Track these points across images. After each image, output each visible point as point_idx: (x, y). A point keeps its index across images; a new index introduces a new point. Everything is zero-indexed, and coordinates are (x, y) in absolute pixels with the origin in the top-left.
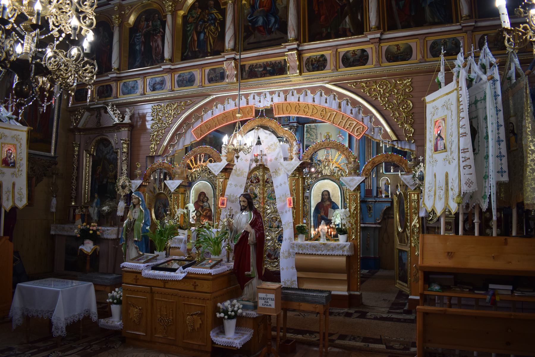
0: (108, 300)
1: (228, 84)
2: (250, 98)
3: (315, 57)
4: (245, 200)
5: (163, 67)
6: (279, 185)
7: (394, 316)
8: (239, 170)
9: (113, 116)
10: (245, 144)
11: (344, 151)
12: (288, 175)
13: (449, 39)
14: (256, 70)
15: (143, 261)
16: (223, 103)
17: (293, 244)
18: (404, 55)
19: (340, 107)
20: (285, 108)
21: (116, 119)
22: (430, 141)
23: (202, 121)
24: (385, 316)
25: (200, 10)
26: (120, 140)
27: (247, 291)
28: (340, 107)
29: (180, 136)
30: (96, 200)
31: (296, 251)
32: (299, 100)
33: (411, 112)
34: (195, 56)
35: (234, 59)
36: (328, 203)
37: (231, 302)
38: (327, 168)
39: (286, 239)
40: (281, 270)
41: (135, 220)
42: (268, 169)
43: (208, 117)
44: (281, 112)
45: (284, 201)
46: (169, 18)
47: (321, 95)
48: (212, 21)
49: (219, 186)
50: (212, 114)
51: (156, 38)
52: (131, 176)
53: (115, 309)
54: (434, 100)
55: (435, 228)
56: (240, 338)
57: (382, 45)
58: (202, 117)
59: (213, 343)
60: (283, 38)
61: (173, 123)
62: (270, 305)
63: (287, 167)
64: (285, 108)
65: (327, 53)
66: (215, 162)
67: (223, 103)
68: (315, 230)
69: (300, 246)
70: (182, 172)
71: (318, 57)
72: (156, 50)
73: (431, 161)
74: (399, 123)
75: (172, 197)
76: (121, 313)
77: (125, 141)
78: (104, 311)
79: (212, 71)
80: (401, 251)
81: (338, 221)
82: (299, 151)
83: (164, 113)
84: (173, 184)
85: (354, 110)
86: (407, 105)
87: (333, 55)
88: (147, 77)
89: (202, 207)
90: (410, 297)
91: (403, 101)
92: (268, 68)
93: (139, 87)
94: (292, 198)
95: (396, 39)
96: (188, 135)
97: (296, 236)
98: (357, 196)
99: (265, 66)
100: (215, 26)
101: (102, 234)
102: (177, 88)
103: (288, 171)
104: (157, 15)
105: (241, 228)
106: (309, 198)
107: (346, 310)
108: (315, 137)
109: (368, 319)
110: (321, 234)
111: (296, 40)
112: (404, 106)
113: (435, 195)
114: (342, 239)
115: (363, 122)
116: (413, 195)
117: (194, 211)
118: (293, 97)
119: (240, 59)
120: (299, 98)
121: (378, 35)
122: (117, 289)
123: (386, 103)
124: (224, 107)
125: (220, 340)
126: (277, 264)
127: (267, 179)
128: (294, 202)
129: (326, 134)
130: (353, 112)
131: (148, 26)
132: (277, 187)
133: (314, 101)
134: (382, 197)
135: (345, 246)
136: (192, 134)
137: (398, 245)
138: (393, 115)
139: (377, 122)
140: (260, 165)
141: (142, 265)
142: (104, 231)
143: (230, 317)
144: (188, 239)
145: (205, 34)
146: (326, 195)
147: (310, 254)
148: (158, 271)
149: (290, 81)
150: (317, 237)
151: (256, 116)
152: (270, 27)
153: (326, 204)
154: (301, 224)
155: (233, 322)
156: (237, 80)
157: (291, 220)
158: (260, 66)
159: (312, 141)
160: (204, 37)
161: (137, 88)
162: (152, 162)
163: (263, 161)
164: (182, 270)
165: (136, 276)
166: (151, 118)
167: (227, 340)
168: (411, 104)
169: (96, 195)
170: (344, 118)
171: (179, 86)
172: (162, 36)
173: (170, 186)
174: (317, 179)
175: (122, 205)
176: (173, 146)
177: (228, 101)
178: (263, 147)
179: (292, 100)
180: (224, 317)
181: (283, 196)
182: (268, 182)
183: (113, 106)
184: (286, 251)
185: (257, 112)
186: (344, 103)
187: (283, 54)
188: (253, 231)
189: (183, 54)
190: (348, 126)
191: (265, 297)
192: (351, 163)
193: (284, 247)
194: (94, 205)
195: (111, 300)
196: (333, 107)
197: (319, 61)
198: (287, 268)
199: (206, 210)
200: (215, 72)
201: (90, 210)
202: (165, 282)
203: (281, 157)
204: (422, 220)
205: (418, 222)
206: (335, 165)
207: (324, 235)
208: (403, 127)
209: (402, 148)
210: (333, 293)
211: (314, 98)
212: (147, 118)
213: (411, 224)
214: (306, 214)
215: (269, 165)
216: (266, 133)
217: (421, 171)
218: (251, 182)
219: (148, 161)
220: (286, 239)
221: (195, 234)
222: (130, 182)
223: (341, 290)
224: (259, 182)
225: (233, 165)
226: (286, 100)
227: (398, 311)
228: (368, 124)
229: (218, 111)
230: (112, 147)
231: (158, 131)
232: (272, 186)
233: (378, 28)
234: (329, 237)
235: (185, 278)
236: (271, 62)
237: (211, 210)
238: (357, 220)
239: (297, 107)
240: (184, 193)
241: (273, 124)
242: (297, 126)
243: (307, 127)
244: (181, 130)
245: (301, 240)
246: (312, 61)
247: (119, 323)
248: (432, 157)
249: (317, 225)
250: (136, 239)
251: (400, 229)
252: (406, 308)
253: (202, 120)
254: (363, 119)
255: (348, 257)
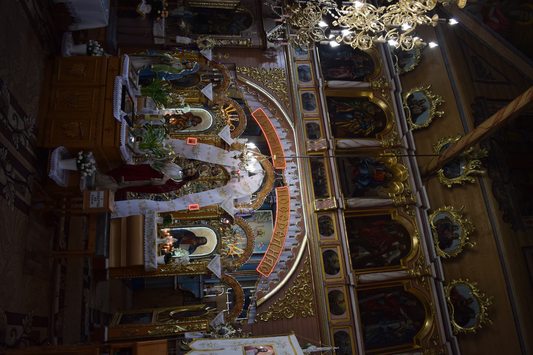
0: (91, 41)
1: (306, 143)
2: (293, 164)
3: (331, 224)
4: (193, 174)
5: (320, 80)
6: (211, 195)
7: (87, 315)
8: (224, 156)
9: (273, 31)
10: (247, 165)
11: (245, 256)
12: (221, 204)
13: (351, 348)
14: (319, 169)
15: (131, 77)
16: (288, 137)
17: (154, 213)
18: (336, 307)
19: (286, 250)
20: (284, 197)
21: (270, 34)
22: (254, 342)
23: (270, 118)
24: (87, 306)
25: (373, 114)
26: (249, 38)
27: (105, 178)
28: (286, 250)
29: (256, 96)
30: (191, 14)
31: (147, 216)
32: (291, 211)
33: (283, 317)
34: (331, 110)
35: (329, 148)
36: (195, 243)
37: (94, 164)
38: (229, 240)
39: (158, 205)
40: (127, 201)
41: (171, 65)
42: (226, 184)
43: (274, 123)
44: (280, 194)
45: (195, 201)
46: (366, 85)
47: (297, 232)
48: (363, 126)
49: (207, 137)
50: (277, 128)
51: (348, 72)
52: (216, 50)
53: (82, 49)
54: (291, 343)
55: (175, 347)
56: (58, 175)
57: (344, 287)
58: (274, 117)
59: (53, 149)
60: (349, 194)
61: (268, 90)
62: (92, 203)
63: (228, 203)
64: (284, 197)
65: (335, 235)
66: (231, 132)
67: (288, 137)
68: (168, 232)
69: (152, 220)
70: (220, 100)
71: (332, 228)
72: (337, 72)
73: (236, 344)
74: (273, 307)
75: (196, 91)
76: (79, 55)
77: (250, 43)
78: (81, 37)
79: (317, 127)
80: (151, 314)
81: (178, 254)
82: (244, 213)
83: (277, 81)
84: (208, 91)
85: (284, 263)
86: (289, 313)
87: (334, 242)
88: (310, 64)
89: (187, 120)
90: (106, 328)
91: (293, 309)
92: (320, 181)
93: (302, 56)
94: (198, 209)
95: (349, 300)
96: (256, 104)
97: (162, 214)
98: (202, 271)
99: (323, 178)
100: (359, 128)
101: (158, 22)
102: (301, 93)
103: (224, 205)
104: (369, 72)
105: (166, 171)
106: (199, 224)
107: (90, 268)
108: (260, 221)
109: (83, 291)
110: (165, 239)
111: (347, 206)
112: (289, 310)
113: (205, 350)
114: (161, 259)
115: (273, 272)
116: (205, 325)
117: (182, 112)
118: (294, 204)
119: (330, 157)
120: (294, 211)
121: (352, 283)
122: (102, 49)
123: (291, 293)
124: (283, 139)
125: (56, 156)
126: (134, 196)
127: (216, 183)
128: (194, 211)
129: (263, 231)
130: (282, 263)
131: (359, 64)
132: (209, 193)
133: (291, 225)
134: (204, 289)
135: (153, 263)
136: (258, 107)
137: (157, 312)
138: (280, 301)
139: (273, 286)
140: (229, 176)
141: (127, 76)
142: (161, 23)
143: (79, 165)
144: (154, 116)
145: (352, 119)
146: (202, 241)
147: (144, 229)
148: (121, 92)
149: (309, 202)
150: (161, 235)
151: (276, 170)
152: (359, 181)
153: (194, 242)
154: (173, 219)
155: (74, 168)
156: (309, 152)
157: (177, 209)
158: (322, 173)
159: (256, 218)
160: (349, 118)
161: (300, 54)
162: (229, 69)
163: (234, 179)
164: (123, 116)
165: (116, 70)
166: (272, 68)
167: (56, 163)
168: (290, 317)
169: (196, 14)
170: (276, 254)
171: (303, 95)
172: (349, 77)
173: (207, 88)
174: (217, 233)
175: (187, 41)
176: (246, 90)
177: (290, 143)
178: (247, 178)
179: (292, 204)
180: (78, 159)
181: (200, 200)
182: (213, 184)
183: (284, 30)
184: (146, 205)
185: (281, 171)
186: (290, 253)
187: (334, 195)
188: (164, 182)
189: (333, 98)
190: (268, 258)
191: (100, 198)
192: (233, 263)
193: (150, 203)
194: (187, 12)
195: (91, 44)
196: (286, 243)
197: (328, 228)
198: (129, 207)
199: (185, 124)
200: (316, 130)
201: (181, 7)
202: (111, 100)
203: (237, 196)
204: (181, 335)
205: (179, 332)
206: (231, 248)
207: (164, 241)
208: (270, 311)
209: (250, 310)
210: (107, 260)
211: (294, 225)
212: (272, 64)
213: (178, 324)
214: (184, 223)
215: (229, 184)
216: (260, 181)
217: (228, 332)
218: (213, 168)
219: (231, 65)
220: (158, 205)
221: (160, 123)
222: (210, 48)
223: (109, 263)
224: (213, 175)
225: (228, 150)
226: (292, 198)
227: (92, 317)
228: (271, 277)
229: (280, 133)
230: (243, 30)
231: (259, 75)
232: (209, 188)
233: (359, 282)
234: (162, 246)
235: (116, 120)
236: (327, 183)
237: (184, 129)
238: (179, 272)
239: (285, 210)
240: (200, 102)
241: (269, 187)
242: (270, 203)
243: (269, 212)
244: (262, 97)
245: (157, 219)
246: (328, 222)
247: (68, 53)
248: (239, 345)
249: (172, 233)
250: (152, 67)
251: (172, 313)
252: (95, 324)
253: (271, 118)
254: (276, 272)
255: (143, 266)
